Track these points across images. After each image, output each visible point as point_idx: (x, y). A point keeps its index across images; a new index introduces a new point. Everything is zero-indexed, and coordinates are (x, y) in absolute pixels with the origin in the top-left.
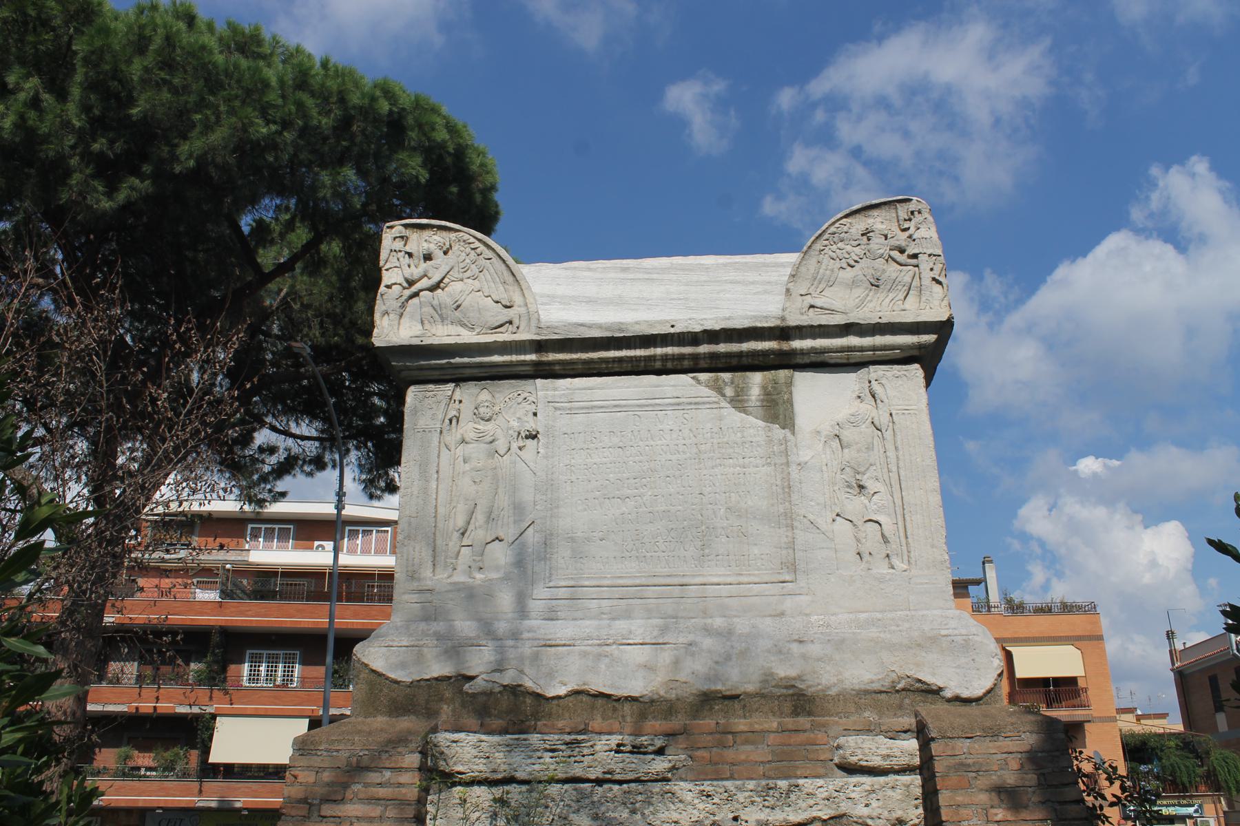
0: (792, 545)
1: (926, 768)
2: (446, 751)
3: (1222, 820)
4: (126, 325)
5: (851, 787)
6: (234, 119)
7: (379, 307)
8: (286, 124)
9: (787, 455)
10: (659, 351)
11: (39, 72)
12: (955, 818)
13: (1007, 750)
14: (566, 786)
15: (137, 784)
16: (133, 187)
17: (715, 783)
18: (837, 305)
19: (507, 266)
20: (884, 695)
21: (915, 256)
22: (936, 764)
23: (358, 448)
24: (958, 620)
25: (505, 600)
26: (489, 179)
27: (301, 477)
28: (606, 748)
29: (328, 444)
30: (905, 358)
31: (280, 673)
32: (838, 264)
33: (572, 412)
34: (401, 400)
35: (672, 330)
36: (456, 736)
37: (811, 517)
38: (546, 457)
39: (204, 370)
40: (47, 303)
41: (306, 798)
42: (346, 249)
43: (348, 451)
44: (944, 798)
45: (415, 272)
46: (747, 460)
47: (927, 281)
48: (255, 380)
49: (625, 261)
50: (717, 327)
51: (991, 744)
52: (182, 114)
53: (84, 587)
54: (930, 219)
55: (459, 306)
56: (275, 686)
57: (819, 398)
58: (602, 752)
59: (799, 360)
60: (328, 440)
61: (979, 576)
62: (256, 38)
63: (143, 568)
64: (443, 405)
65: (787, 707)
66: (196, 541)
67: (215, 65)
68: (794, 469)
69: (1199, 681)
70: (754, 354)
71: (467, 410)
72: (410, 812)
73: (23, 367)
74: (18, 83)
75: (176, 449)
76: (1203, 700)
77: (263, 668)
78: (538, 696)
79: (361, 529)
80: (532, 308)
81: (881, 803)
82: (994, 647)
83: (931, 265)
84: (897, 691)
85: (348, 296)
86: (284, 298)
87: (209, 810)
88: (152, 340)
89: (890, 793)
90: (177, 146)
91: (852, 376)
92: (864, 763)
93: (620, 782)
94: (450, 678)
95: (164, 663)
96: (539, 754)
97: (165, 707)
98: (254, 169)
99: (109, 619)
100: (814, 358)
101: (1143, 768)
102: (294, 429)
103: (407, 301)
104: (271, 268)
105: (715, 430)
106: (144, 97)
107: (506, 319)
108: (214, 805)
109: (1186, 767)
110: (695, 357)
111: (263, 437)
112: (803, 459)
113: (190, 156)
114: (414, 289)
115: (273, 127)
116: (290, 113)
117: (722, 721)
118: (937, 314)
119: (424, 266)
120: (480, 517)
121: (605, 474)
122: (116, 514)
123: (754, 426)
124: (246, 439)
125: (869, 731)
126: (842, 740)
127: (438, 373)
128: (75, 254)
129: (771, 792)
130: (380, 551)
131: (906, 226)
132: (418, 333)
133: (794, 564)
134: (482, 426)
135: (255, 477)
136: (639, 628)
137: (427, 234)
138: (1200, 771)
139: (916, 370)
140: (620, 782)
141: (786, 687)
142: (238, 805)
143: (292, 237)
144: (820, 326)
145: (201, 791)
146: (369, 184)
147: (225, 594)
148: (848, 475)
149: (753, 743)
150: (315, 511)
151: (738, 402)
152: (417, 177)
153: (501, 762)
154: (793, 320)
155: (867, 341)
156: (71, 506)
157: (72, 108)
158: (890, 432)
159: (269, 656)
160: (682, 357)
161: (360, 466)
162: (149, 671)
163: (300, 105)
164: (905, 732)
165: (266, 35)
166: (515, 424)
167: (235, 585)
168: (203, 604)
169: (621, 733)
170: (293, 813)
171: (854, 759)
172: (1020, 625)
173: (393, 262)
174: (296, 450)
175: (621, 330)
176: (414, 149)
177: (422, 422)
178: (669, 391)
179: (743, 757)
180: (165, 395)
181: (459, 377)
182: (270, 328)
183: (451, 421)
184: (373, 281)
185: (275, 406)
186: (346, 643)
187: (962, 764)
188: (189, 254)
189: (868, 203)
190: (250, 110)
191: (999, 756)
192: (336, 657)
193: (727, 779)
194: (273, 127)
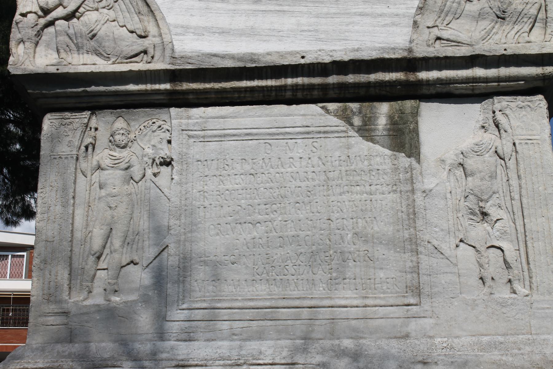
0: (416, 270)
7: (15, 35)
9: (412, 183)
10: (290, 81)
18: (463, 37)
25: (144, 320)
30: (528, 88)
33: (205, 140)
35: (303, 61)
37: (435, 243)
38: (180, 184)
46: (373, 188)
50: (346, 58)
55: (94, 36)
64: (78, 133)
68: (419, 196)
71: (103, 136)
80: (167, 38)
91: (477, 106)
100: (439, 89)
103: (43, 29)
110: (324, 87)
114: (49, 17)
120: (117, 242)
123: (380, 154)
130: (15, 276)
133: (418, 288)
134: (117, 153)
144: (446, 58)
148: (472, 202)
151: (366, 131)
154: (421, 51)
155: (492, 72)
160: (311, 87)
175: (252, 61)
177: (63, 149)
178: (299, 121)
181: (96, 105)
183: (87, 147)
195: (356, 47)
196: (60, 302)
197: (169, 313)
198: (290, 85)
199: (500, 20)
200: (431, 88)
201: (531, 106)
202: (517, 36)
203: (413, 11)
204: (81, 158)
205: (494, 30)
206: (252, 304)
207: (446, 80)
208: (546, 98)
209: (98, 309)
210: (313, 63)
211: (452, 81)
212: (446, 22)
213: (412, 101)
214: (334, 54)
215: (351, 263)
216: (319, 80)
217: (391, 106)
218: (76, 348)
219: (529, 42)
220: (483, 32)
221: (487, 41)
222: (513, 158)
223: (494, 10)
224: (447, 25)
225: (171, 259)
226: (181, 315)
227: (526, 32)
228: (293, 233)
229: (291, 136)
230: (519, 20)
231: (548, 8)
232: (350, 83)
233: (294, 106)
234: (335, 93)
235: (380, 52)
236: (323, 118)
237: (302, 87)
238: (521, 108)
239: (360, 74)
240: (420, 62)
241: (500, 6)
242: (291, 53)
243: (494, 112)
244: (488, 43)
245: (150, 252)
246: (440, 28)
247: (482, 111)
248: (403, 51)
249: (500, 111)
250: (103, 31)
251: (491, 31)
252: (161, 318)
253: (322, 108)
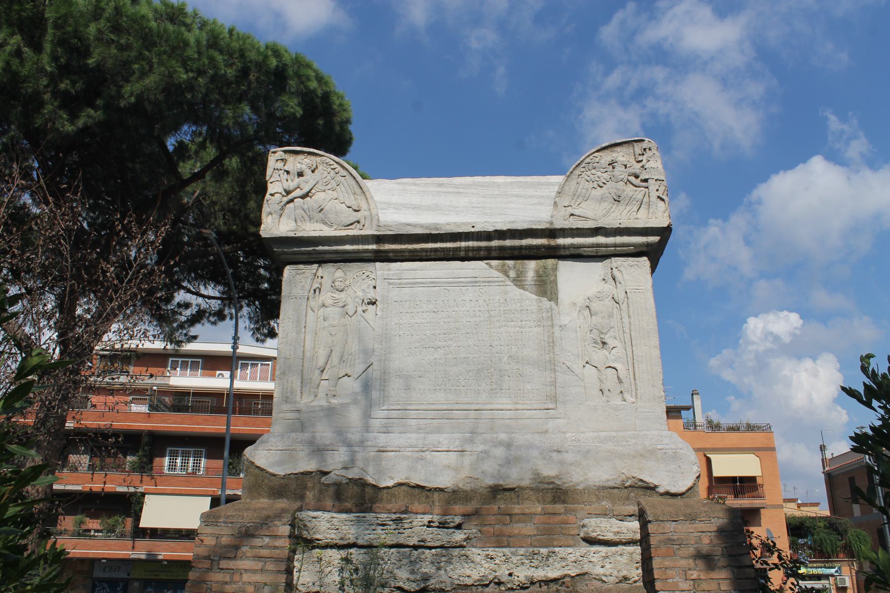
0: (554, 383)
1: (644, 541)
2: (308, 524)
3: (854, 578)
4: (84, 215)
5: (592, 554)
6: (163, 69)
7: (266, 209)
8: (200, 72)
9: (552, 320)
10: (463, 244)
11: (21, 31)
12: (664, 577)
13: (704, 530)
14: (393, 550)
15: (89, 541)
16: (90, 116)
17: (497, 549)
18: (590, 214)
19: (357, 182)
20: (616, 491)
21: (646, 181)
22: (651, 539)
23: (248, 305)
24: (669, 437)
25: (354, 416)
26: (345, 115)
27: (208, 325)
28: (421, 524)
29: (227, 302)
30: (637, 253)
31: (191, 465)
32: (591, 185)
33: (401, 286)
34: (280, 273)
35: (473, 230)
36: (315, 514)
37: (568, 364)
38: (382, 318)
39: (141, 248)
40: (26, 198)
41: (209, 556)
42: (243, 163)
43: (241, 307)
44: (656, 563)
45: (291, 185)
46: (523, 323)
47: (654, 198)
48: (177, 259)
49: (440, 179)
50: (505, 228)
51: (690, 526)
52: (126, 64)
53: (53, 404)
54: (657, 154)
55: (322, 210)
56: (187, 473)
57: (576, 280)
58: (418, 526)
59: (562, 253)
60: (227, 299)
61: (689, 404)
62: (181, 10)
63: (92, 389)
64: (309, 280)
65: (549, 496)
66: (131, 369)
67: (151, 29)
68: (557, 329)
69: (839, 482)
70: (530, 247)
71: (327, 283)
72: (283, 567)
73: (11, 247)
74: (5, 40)
75: (120, 308)
76: (845, 492)
77: (179, 461)
78: (375, 487)
79: (250, 362)
80: (374, 212)
81: (612, 565)
82: (693, 456)
83: (657, 187)
84: (626, 488)
85: (243, 198)
86: (198, 197)
87: (139, 560)
88: (103, 226)
89: (619, 558)
90: (122, 87)
91: (600, 264)
92: (601, 538)
93: (430, 548)
94: (312, 473)
95: (109, 456)
96: (373, 527)
97: (110, 487)
98: (177, 104)
99: (70, 425)
100: (573, 251)
101: (800, 541)
102: (203, 291)
103: (285, 205)
104: (189, 176)
105: (502, 301)
106: (97, 51)
107: (356, 220)
108: (143, 557)
109: (831, 541)
110: (489, 249)
111: (181, 296)
112: (563, 322)
113: (132, 94)
114: (290, 197)
115: (191, 75)
116: (204, 65)
117: (503, 506)
118: (661, 221)
119: (297, 180)
120: (335, 359)
121: (426, 335)
122: (76, 349)
123: (529, 299)
124: (169, 299)
125: (606, 515)
126: (586, 521)
127: (306, 257)
128: (47, 164)
129: (536, 556)
130: (263, 379)
131: (640, 159)
132: (293, 228)
133: (555, 397)
134: (337, 295)
135: (175, 325)
136: (444, 440)
137: (300, 157)
138: (839, 543)
139: (645, 261)
140: (430, 548)
141: (548, 483)
142: (160, 557)
143: (203, 154)
144: (578, 229)
145: (133, 547)
146: (260, 117)
147: (152, 407)
148: (595, 335)
149: (524, 522)
150: (217, 350)
151: (519, 281)
152: (294, 114)
153: (350, 532)
154: (558, 225)
155: (610, 240)
156: (44, 347)
157: (45, 59)
158: (625, 304)
159: (183, 452)
160: (479, 249)
161: (250, 318)
162: (97, 462)
163: (212, 59)
164: (631, 516)
165: (189, 10)
166: (360, 294)
167: (159, 401)
168: (137, 415)
169: (431, 514)
170: (200, 566)
171: (594, 535)
172: (716, 439)
173: (276, 177)
174: (204, 306)
175: (437, 229)
176: (293, 93)
177: (297, 291)
178: (470, 273)
179: (516, 532)
180: (112, 269)
181: (321, 260)
182: (187, 218)
183: (315, 291)
184: (261, 189)
185: (189, 274)
186: (240, 444)
187: (669, 539)
188: (130, 165)
189: (613, 142)
190: (174, 62)
191: (695, 534)
192: (230, 454)
193: (505, 547)
194: (191, 75)
196: (295, 402)
197: (373, 413)
203: (554, 194)
204: (310, 298)
206: (433, 407)
209: (322, 409)
214: (496, 224)
215: (506, 378)
218: (306, 436)
222: (625, 303)
225: (375, 371)
226: (383, 414)
228: (464, 356)
229: (465, 285)
242: (464, 224)
245: (360, 368)
250: (328, 207)
252: (367, 415)
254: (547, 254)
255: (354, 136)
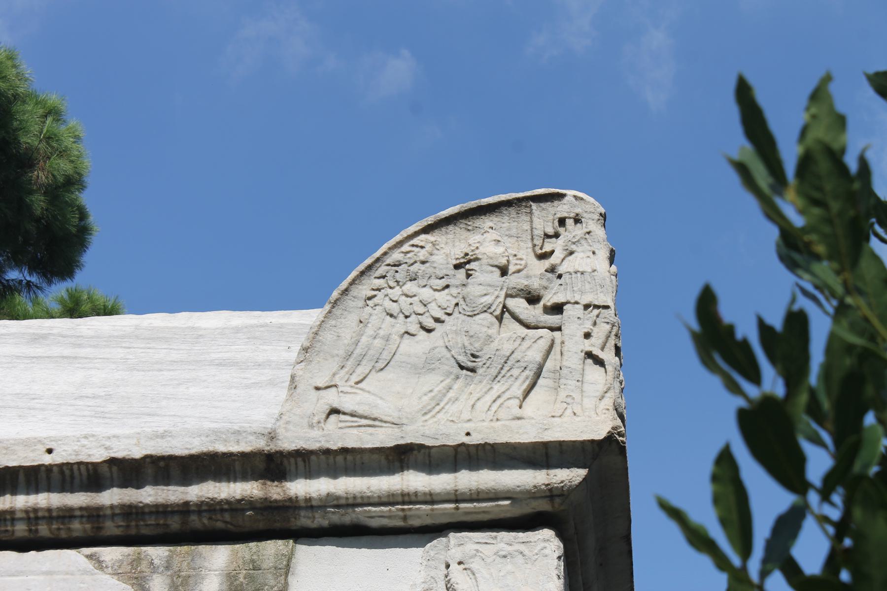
18: (384, 408)
21: (557, 309)
32: (400, 325)
35: (47, 460)
47: (573, 358)
50: (137, 453)
54: (599, 232)
59: (305, 520)
70: (212, 507)
83: (587, 326)
100: (335, 517)
110: (94, 514)
118: (593, 424)
131: (547, 248)
144: (344, 451)
154: (288, 443)
160: (67, 514)
195: (161, 430)
198: (21, 511)
199: (465, 372)
200: (317, 515)
201: (526, 552)
202: (495, 407)
205: (451, 394)
207: (347, 498)
208: (560, 535)
210: (68, 464)
211: (359, 501)
212: (355, 378)
213: (280, 542)
216: (83, 498)
217: (235, 553)
219: (519, 418)
220: (426, 398)
221: (434, 416)
223: (453, 352)
224: (357, 383)
227: (515, 397)
230: (503, 372)
231: (565, 349)
232: (147, 505)
233: (33, 553)
234: (118, 527)
235: (208, 439)
236: (87, 578)
237: (46, 514)
238: (505, 557)
239: (167, 484)
240: (292, 460)
241: (467, 344)
242: (27, 443)
243: (448, 566)
244: (435, 420)
246: (340, 389)
247: (425, 563)
248: (257, 438)
249: (460, 563)
251: (445, 395)
253: (90, 557)
254: (261, 526)
255: (93, 219)
